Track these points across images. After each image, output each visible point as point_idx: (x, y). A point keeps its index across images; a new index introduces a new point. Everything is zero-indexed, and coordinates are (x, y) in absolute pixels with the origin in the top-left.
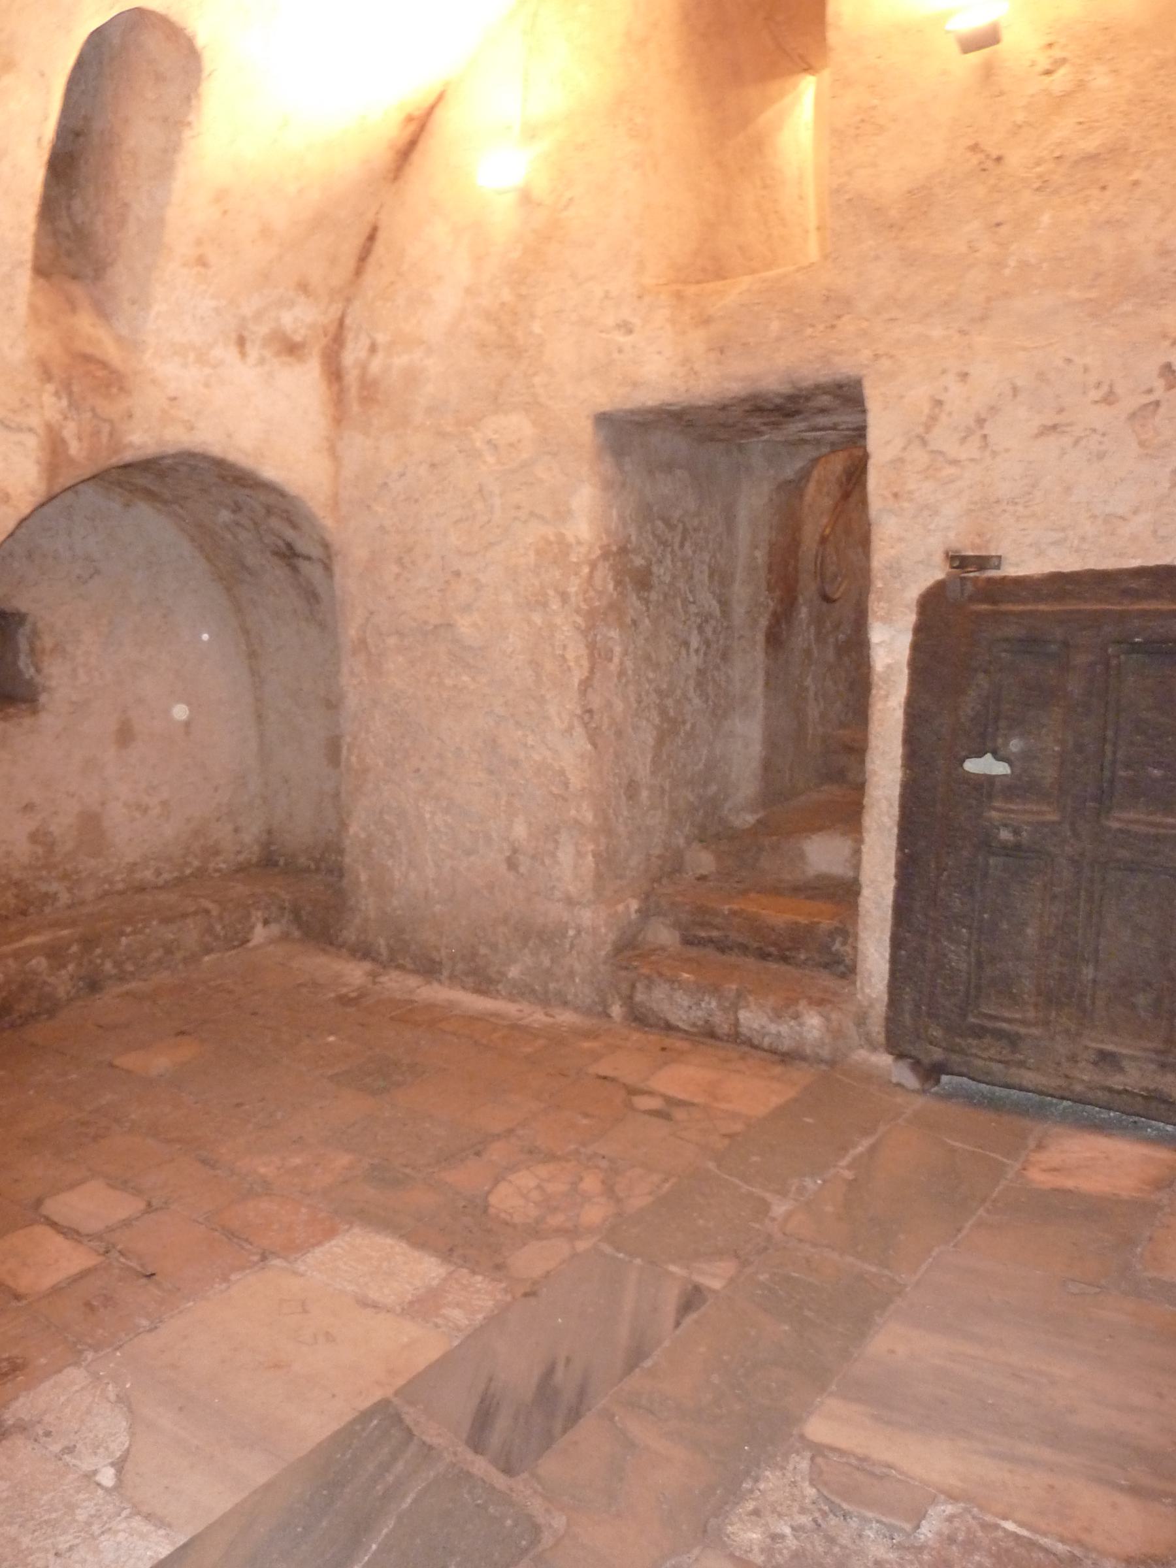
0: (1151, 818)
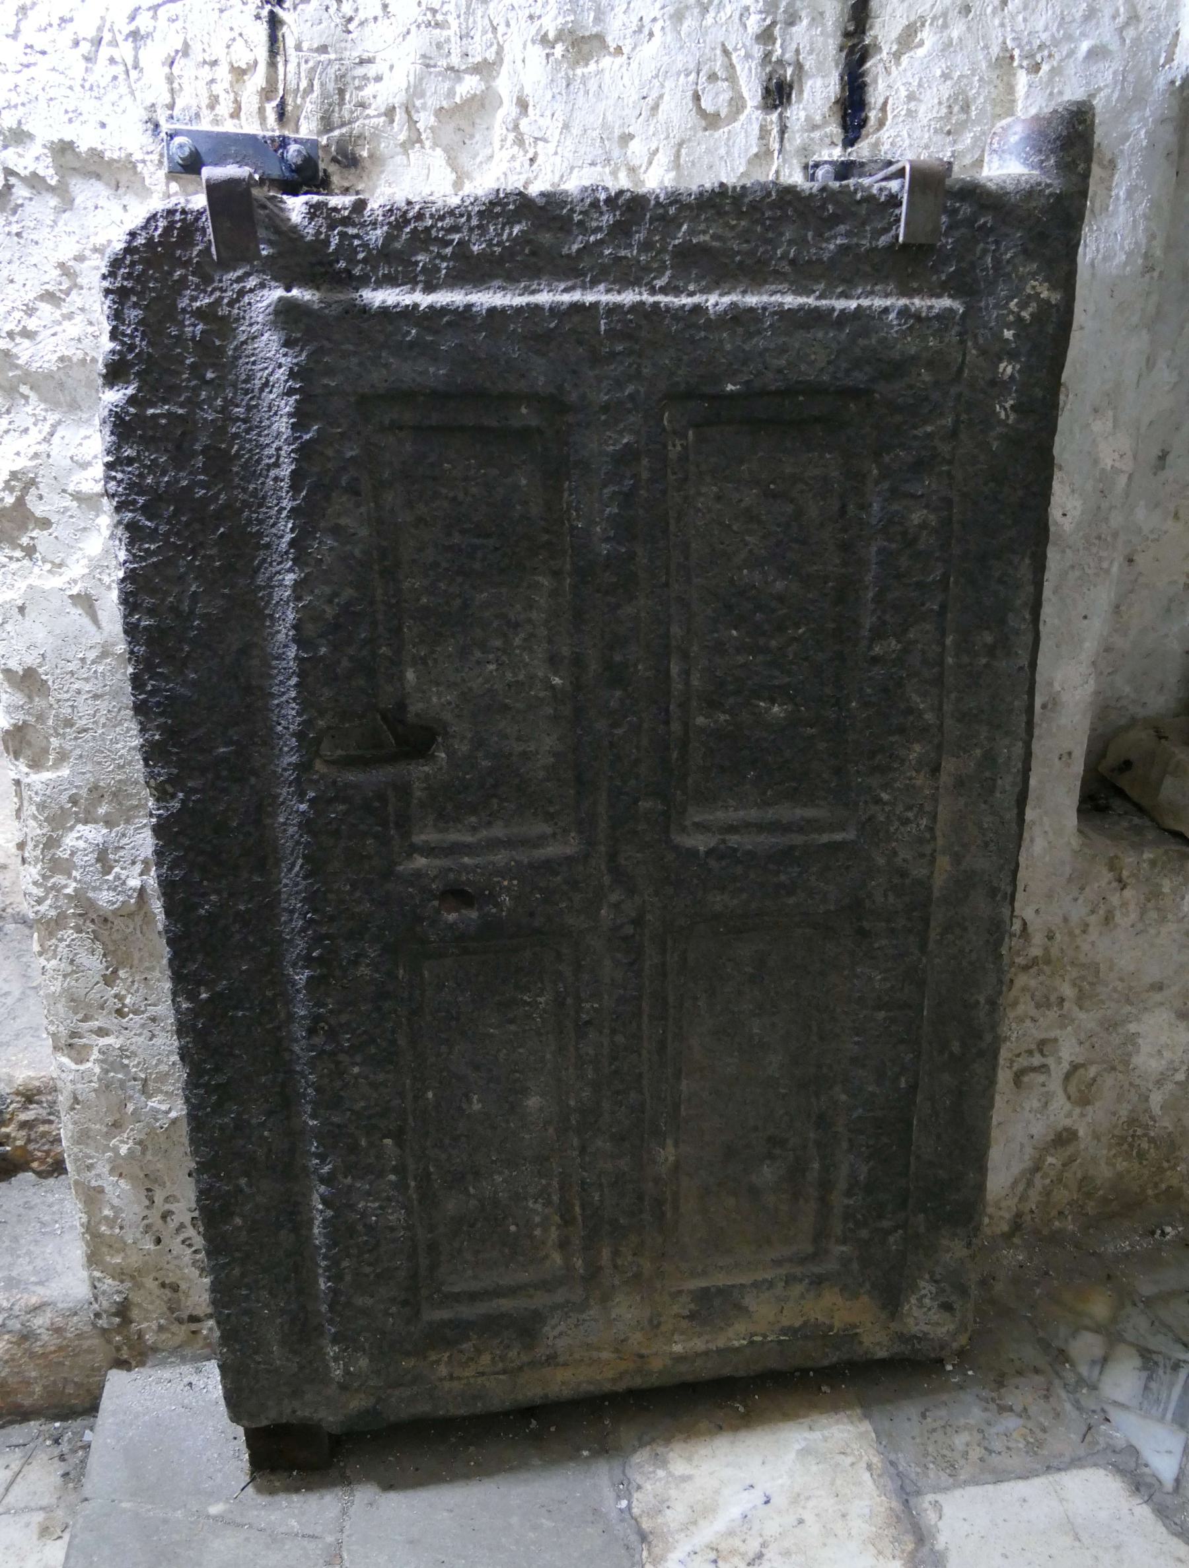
0: (770, 814)
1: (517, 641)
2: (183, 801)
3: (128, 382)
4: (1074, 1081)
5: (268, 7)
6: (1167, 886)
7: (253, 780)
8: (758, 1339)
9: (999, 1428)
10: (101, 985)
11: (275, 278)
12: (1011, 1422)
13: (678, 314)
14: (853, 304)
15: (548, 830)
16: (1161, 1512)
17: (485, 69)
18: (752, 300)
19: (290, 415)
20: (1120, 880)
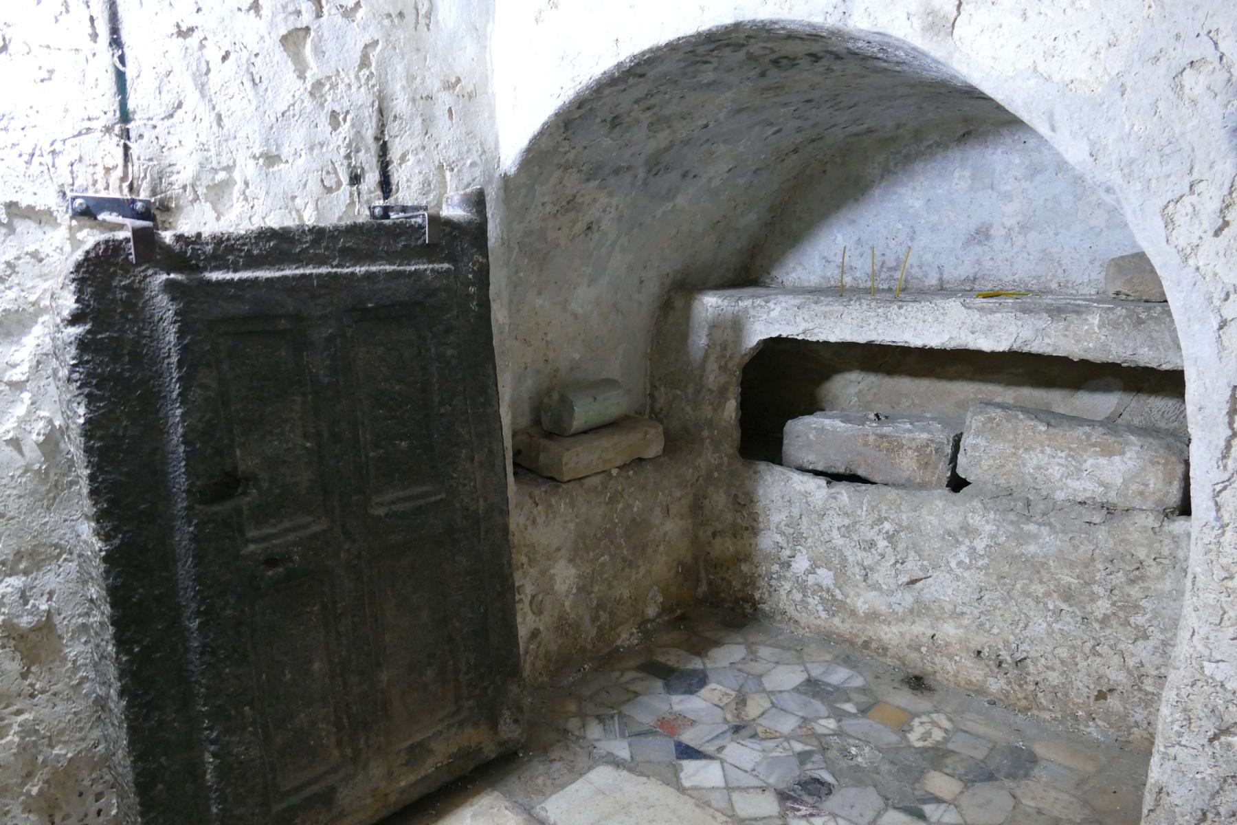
1: (287, 429)
2: (122, 539)
3: (85, 323)
4: (534, 603)
5: (123, 141)
6: (553, 501)
7: (159, 520)
8: (439, 765)
9: (554, 769)
10: (19, 680)
11: (162, 269)
12: (557, 765)
13: (345, 276)
14: (413, 268)
15: (310, 519)
16: (631, 770)
17: (229, 169)
18: (374, 268)
19: (176, 333)
20: (535, 502)
